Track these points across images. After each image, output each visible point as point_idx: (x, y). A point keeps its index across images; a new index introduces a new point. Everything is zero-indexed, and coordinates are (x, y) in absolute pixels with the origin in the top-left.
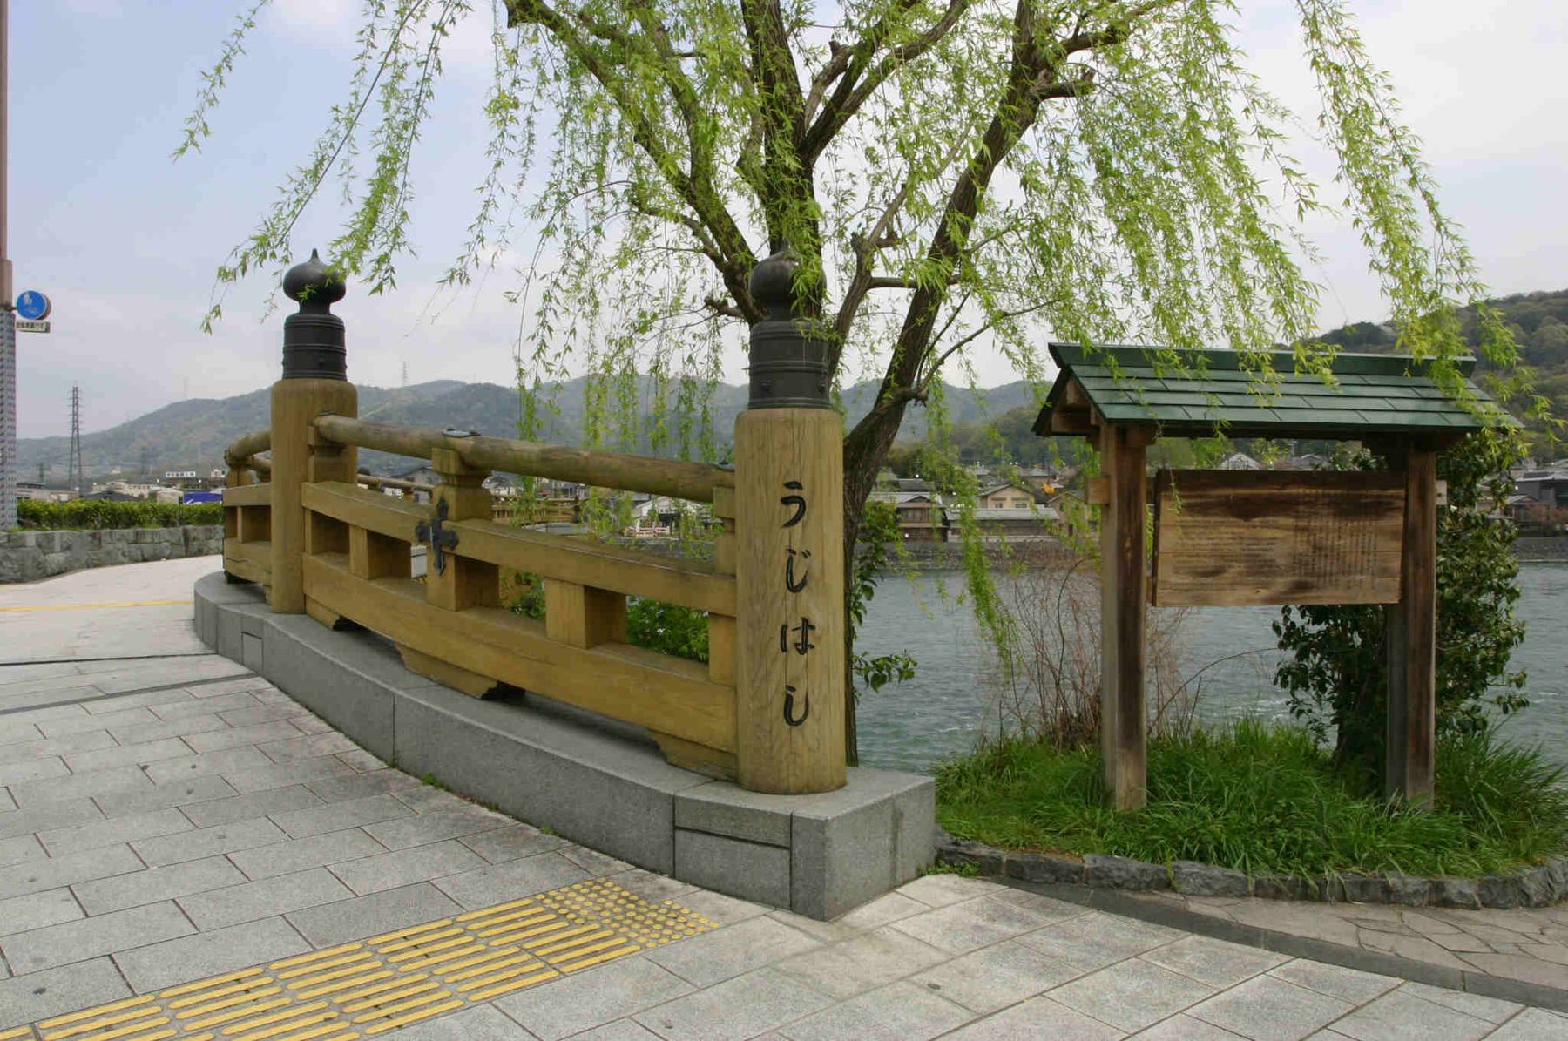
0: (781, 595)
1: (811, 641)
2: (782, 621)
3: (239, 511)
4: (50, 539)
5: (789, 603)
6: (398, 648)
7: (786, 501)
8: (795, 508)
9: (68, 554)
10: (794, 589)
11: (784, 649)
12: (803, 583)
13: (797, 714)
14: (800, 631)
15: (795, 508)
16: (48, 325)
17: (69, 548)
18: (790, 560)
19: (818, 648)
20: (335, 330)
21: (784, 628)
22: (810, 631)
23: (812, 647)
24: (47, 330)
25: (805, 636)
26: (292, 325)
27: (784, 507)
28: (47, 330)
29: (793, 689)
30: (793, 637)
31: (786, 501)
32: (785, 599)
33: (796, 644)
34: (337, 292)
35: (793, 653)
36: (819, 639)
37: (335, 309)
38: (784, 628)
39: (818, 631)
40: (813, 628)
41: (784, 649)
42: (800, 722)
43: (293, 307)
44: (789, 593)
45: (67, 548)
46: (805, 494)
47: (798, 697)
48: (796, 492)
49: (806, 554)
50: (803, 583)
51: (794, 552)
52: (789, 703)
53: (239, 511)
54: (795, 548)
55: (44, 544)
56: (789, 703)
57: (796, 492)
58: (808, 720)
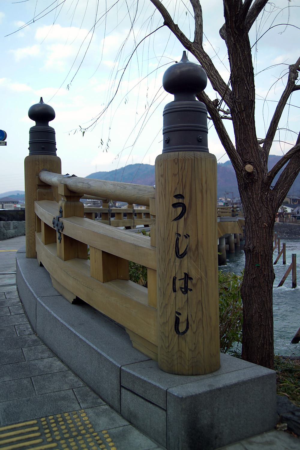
0: (172, 260)
1: (190, 286)
2: (174, 275)
3: (143, 214)
4: (9, 224)
5: (177, 264)
6: (51, 277)
7: (175, 205)
8: (180, 210)
9: (16, 230)
10: (181, 256)
11: (175, 291)
12: (185, 253)
13: (182, 328)
14: (183, 281)
15: (180, 210)
16: (6, 142)
17: (16, 228)
18: (177, 240)
19: (194, 290)
20: (52, 132)
21: (174, 279)
22: (189, 281)
23: (191, 290)
24: (6, 145)
25: (186, 283)
26: (33, 131)
27: (174, 209)
28: (6, 145)
29: (180, 314)
30: (179, 284)
31: (175, 205)
32: (175, 262)
33: (181, 288)
34: (51, 116)
35: (179, 293)
36: (195, 285)
37: (51, 124)
38: (174, 279)
39: (194, 281)
40: (191, 279)
41: (175, 291)
42: (184, 333)
43: (33, 123)
44: (177, 259)
45: (15, 228)
46: (186, 202)
47: (182, 319)
48: (181, 201)
49: (187, 236)
50: (185, 253)
51: (180, 235)
52: (177, 322)
53: (143, 214)
54: (180, 232)
55: (6, 226)
56: (177, 322)
57: (181, 201)
58: (189, 332)
